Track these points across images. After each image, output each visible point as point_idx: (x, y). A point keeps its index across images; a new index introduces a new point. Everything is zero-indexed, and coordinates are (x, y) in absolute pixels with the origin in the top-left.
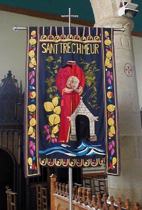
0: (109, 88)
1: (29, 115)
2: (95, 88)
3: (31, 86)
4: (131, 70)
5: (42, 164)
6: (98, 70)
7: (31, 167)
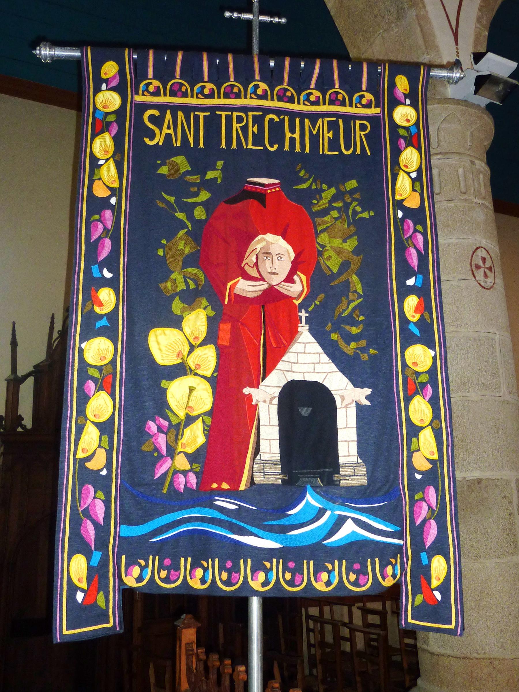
0: (410, 282)
1: (84, 377)
2: (355, 278)
3: (95, 269)
4: (490, 269)
5: (130, 582)
6: (365, 215)
7: (80, 597)
